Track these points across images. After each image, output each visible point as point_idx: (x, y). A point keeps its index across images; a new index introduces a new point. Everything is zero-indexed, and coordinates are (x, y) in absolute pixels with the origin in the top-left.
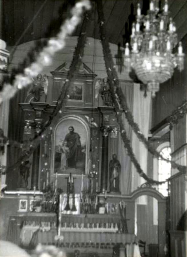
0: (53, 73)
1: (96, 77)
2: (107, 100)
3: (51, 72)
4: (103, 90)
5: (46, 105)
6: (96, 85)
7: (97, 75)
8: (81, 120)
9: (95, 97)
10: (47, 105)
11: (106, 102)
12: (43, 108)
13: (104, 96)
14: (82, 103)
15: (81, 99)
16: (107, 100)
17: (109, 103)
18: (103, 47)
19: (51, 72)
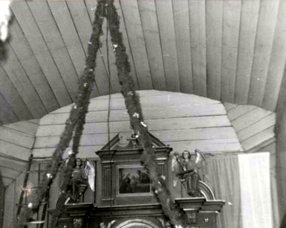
0: (101, 154)
1: (172, 153)
2: (191, 188)
3: (98, 153)
4: (183, 170)
5: (201, 201)
6: (173, 166)
7: (171, 149)
8: (126, 225)
9: (173, 184)
10: (203, 201)
11: (190, 191)
12: (84, 212)
13: (185, 181)
14: (151, 196)
15: (148, 191)
16: (191, 188)
17: (193, 192)
18: (79, 139)
19: (98, 153)
